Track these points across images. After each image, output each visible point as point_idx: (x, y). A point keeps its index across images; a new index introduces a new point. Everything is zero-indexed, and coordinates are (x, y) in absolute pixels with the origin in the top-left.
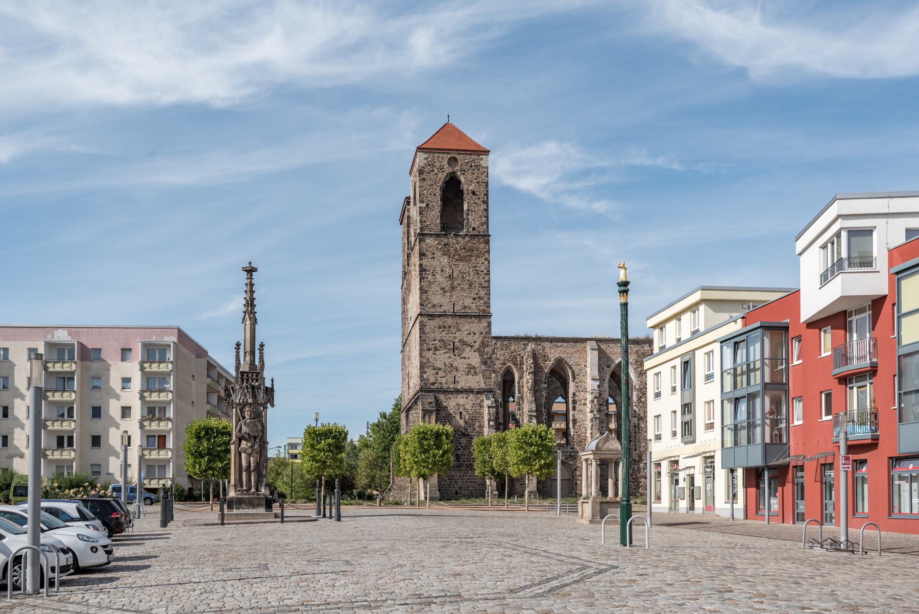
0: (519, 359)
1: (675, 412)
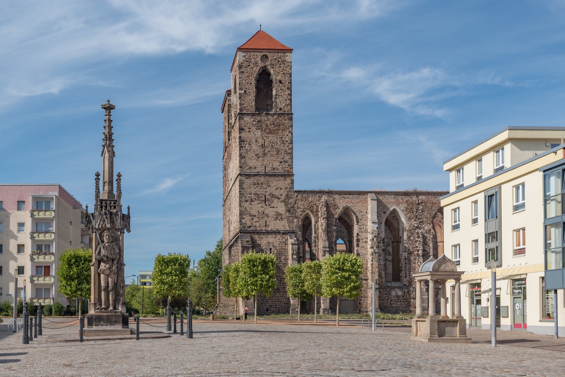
0: (315, 207)
1: (476, 241)
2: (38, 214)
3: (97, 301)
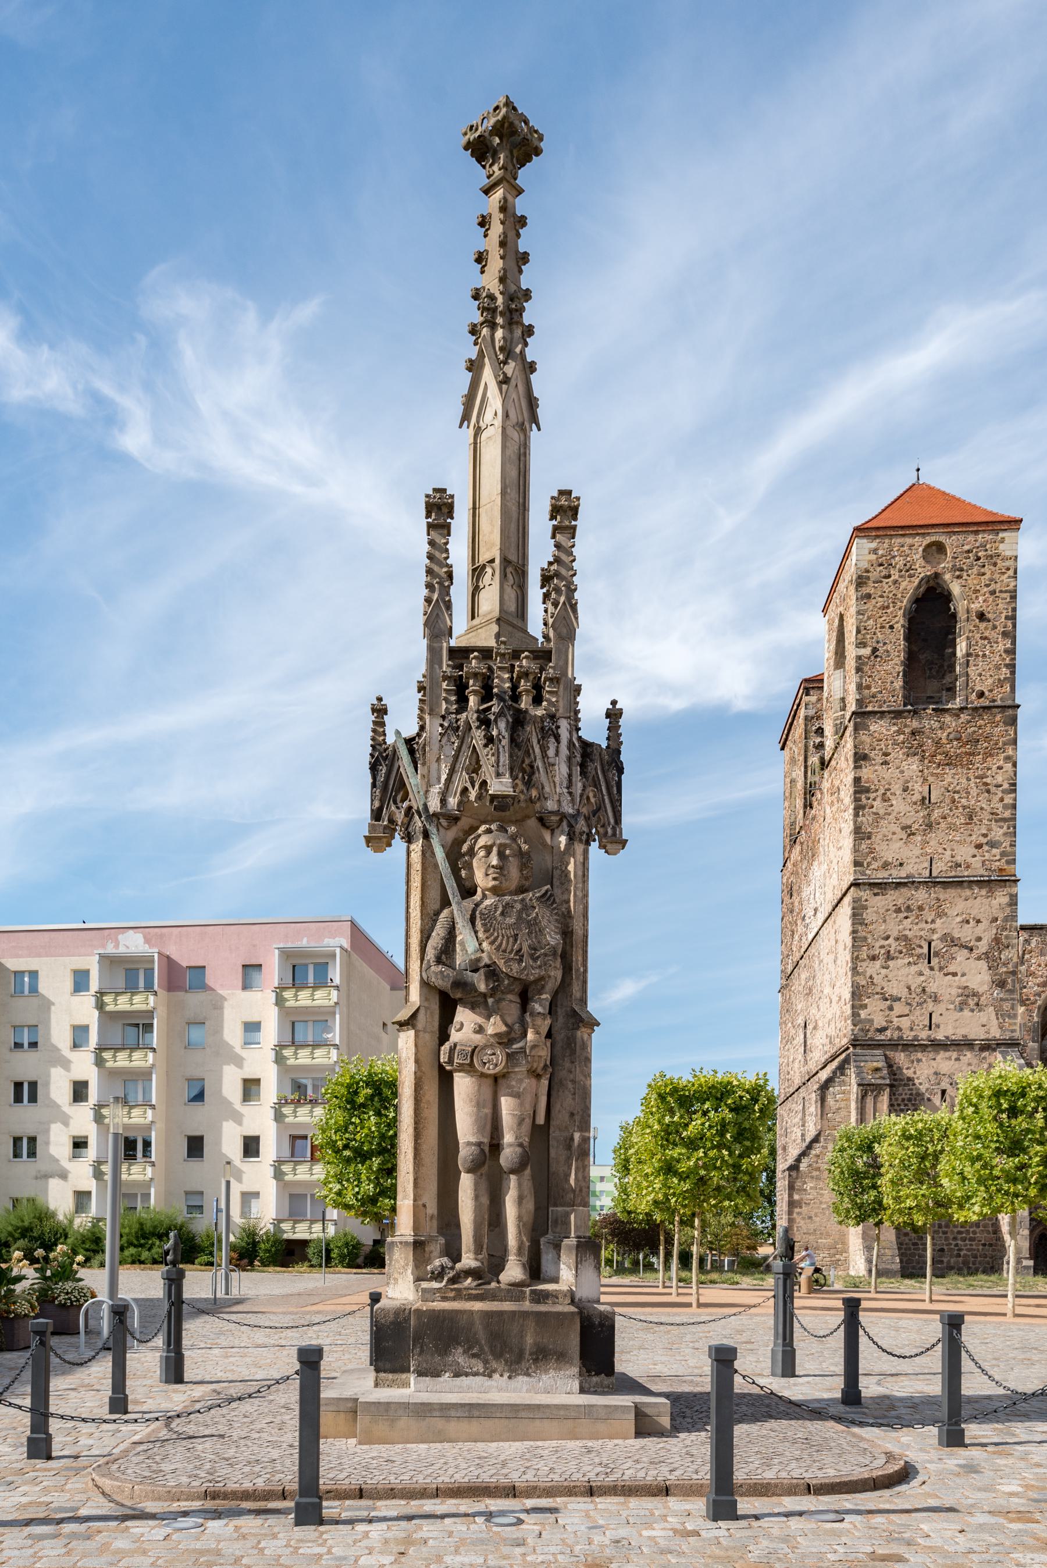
3: (431, 1228)
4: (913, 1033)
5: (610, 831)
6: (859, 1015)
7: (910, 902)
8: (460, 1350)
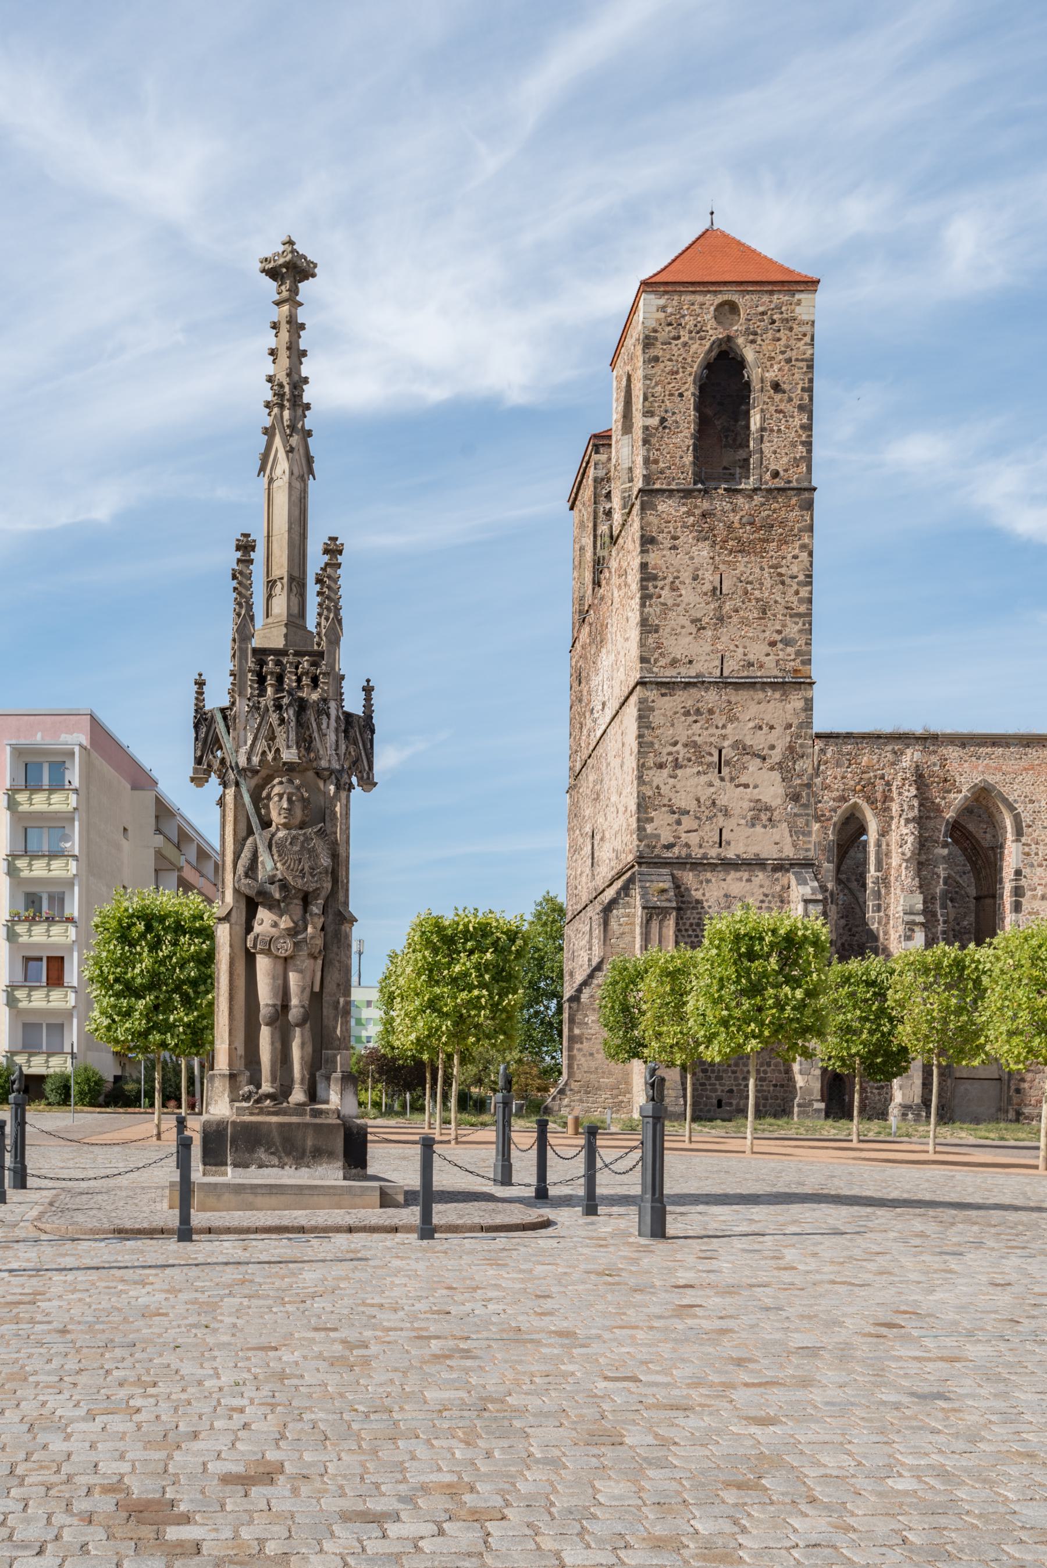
0: (880, 786)
2: (30, 799)
3: (240, 1065)
4: (702, 851)
5: (365, 775)
6: (645, 830)
7: (700, 705)
8: (263, 1149)
